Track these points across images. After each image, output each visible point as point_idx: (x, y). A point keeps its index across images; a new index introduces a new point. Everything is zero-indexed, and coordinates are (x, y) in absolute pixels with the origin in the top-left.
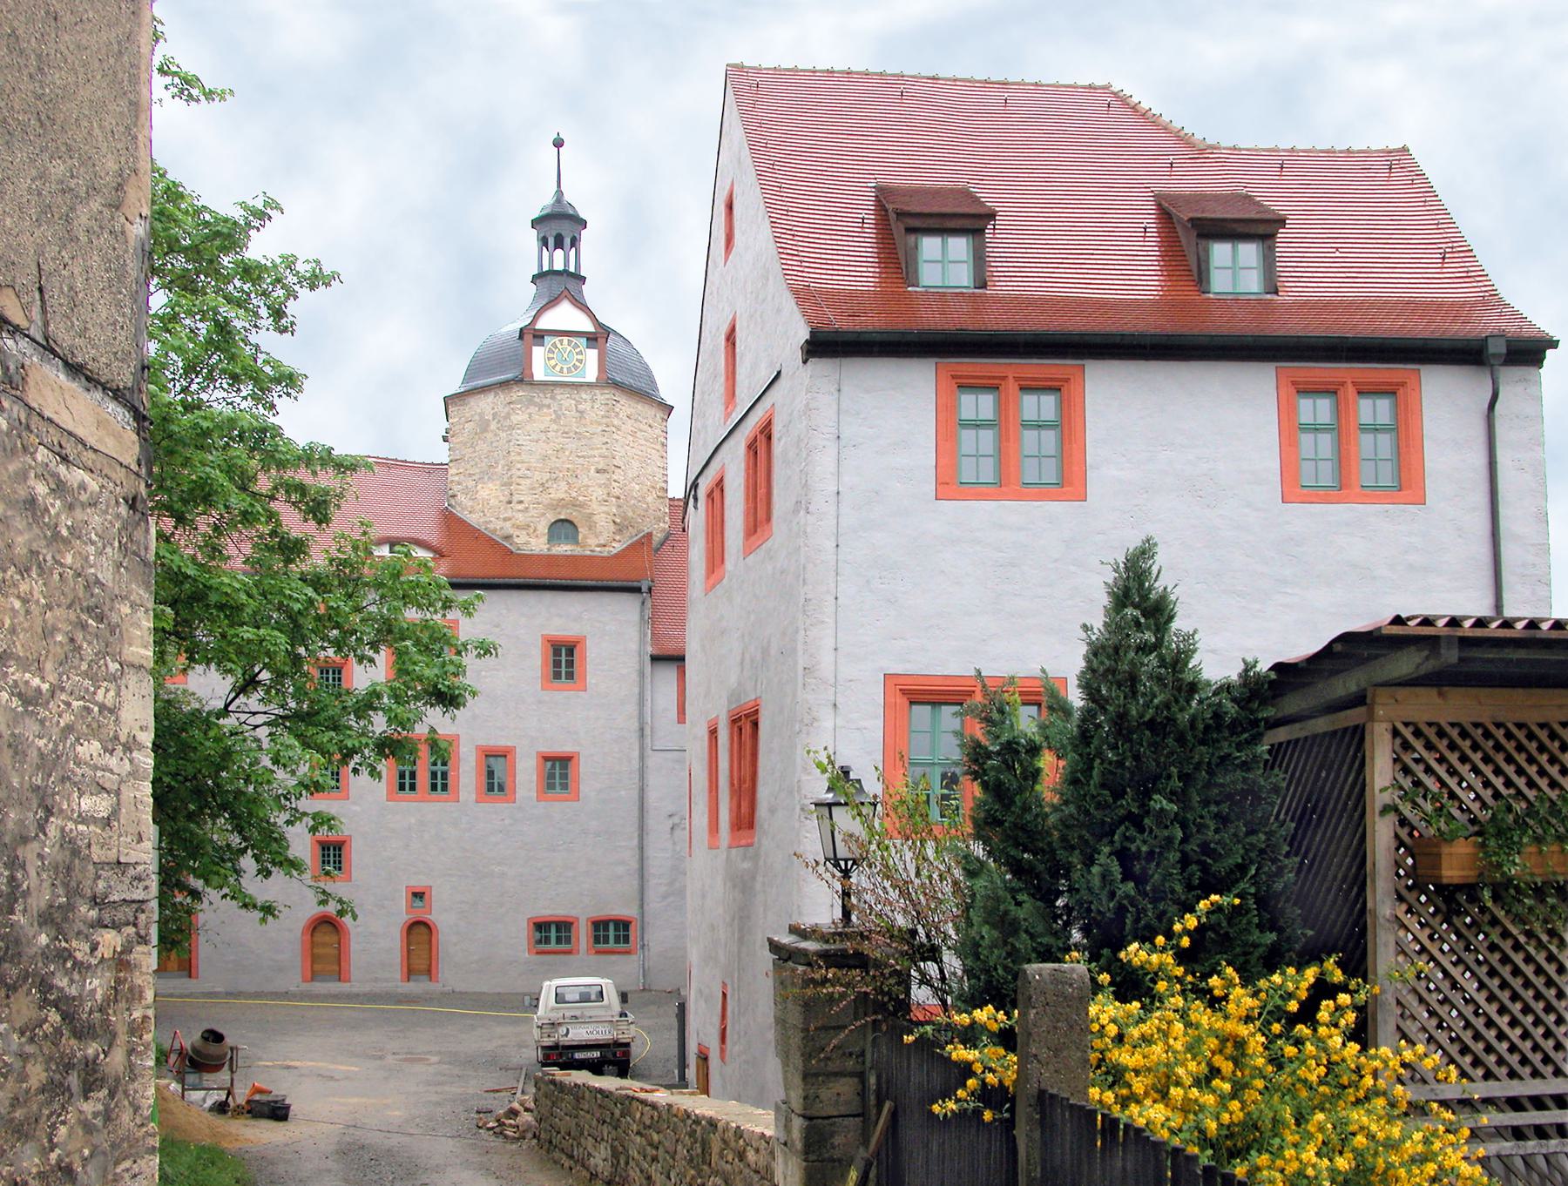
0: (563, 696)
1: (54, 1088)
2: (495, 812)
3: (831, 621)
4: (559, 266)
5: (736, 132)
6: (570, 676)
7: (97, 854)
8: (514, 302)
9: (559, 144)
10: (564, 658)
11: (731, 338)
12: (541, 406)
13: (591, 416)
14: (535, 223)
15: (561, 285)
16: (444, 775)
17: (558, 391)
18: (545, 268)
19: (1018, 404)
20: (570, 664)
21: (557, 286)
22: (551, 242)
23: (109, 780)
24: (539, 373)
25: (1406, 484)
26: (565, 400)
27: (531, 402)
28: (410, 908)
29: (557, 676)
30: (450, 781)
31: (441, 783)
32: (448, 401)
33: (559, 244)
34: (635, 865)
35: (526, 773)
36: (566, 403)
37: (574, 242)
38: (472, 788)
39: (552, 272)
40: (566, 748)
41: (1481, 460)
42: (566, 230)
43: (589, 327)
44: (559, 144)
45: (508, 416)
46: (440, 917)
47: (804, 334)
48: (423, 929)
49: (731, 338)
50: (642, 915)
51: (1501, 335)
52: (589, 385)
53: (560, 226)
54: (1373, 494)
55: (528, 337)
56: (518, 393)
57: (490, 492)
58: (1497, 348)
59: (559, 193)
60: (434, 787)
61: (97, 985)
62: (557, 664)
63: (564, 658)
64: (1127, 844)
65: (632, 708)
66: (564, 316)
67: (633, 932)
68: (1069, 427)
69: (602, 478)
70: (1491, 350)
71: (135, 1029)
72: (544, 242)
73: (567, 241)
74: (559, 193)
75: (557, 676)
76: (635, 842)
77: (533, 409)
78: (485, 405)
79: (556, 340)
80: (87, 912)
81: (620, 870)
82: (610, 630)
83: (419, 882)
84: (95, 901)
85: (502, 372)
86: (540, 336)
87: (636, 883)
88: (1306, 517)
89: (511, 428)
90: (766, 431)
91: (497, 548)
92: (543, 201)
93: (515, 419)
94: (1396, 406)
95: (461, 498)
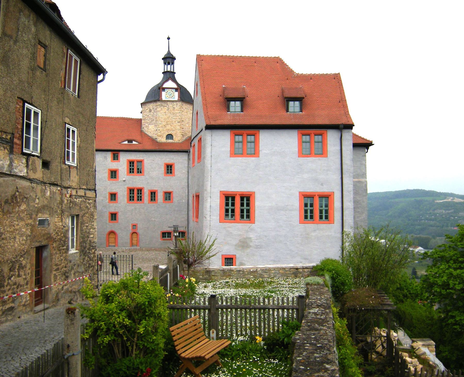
0: (169, 177)
1: (89, 267)
2: (153, 206)
3: (210, 181)
4: (169, 70)
5: (197, 71)
6: (171, 173)
7: (92, 241)
8: (159, 78)
9: (169, 38)
10: (169, 169)
11: (197, 113)
12: (164, 106)
13: (176, 108)
14: (163, 59)
15: (169, 75)
16: (141, 197)
17: (168, 103)
18: (166, 70)
19: (247, 138)
20: (171, 170)
21: (168, 75)
22: (167, 64)
23: (93, 233)
24: (164, 98)
25: (323, 153)
26: (170, 105)
27: (162, 105)
28: (133, 229)
29: (168, 173)
30: (142, 199)
31: (140, 199)
32: (142, 104)
33: (169, 64)
34: (187, 218)
35: (160, 196)
36: (170, 106)
37: (173, 63)
38: (147, 200)
39: (167, 72)
40: (170, 190)
41: (339, 148)
42: (170, 60)
43: (175, 86)
44: (169, 38)
45: (156, 109)
46: (140, 231)
47: (205, 125)
48: (135, 234)
49: (197, 113)
50: (188, 230)
51: (343, 124)
52: (176, 101)
53: (169, 59)
54: (317, 155)
55: (161, 89)
56: (159, 103)
57: (152, 127)
58: (342, 126)
59: (169, 50)
60: (138, 200)
61: (92, 256)
62: (168, 170)
63: (169, 169)
64: (107, 267)
65: (186, 181)
66: (170, 84)
67: (186, 235)
68: (256, 142)
69: (179, 124)
70: (340, 127)
71: (95, 260)
72: (165, 63)
73: (171, 64)
74: (169, 50)
75: (168, 173)
76: (187, 213)
77: (162, 107)
78: (151, 106)
79: (168, 90)
80: (91, 248)
81: (183, 219)
82: (179, 161)
83: (135, 222)
84: (92, 246)
85: (155, 96)
86: (164, 89)
87: (187, 222)
88: (302, 160)
89: (157, 112)
90: (201, 139)
91: (153, 141)
92: (164, 53)
93: (158, 110)
94: (322, 137)
95: (145, 128)
